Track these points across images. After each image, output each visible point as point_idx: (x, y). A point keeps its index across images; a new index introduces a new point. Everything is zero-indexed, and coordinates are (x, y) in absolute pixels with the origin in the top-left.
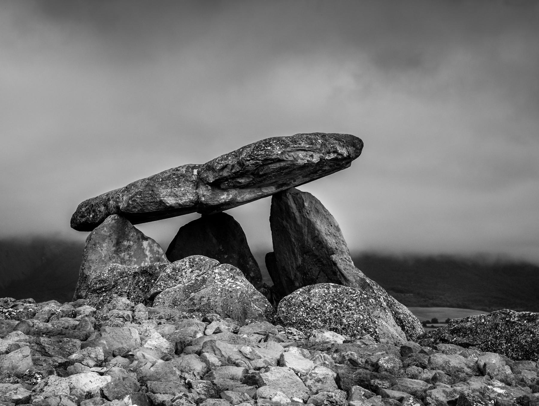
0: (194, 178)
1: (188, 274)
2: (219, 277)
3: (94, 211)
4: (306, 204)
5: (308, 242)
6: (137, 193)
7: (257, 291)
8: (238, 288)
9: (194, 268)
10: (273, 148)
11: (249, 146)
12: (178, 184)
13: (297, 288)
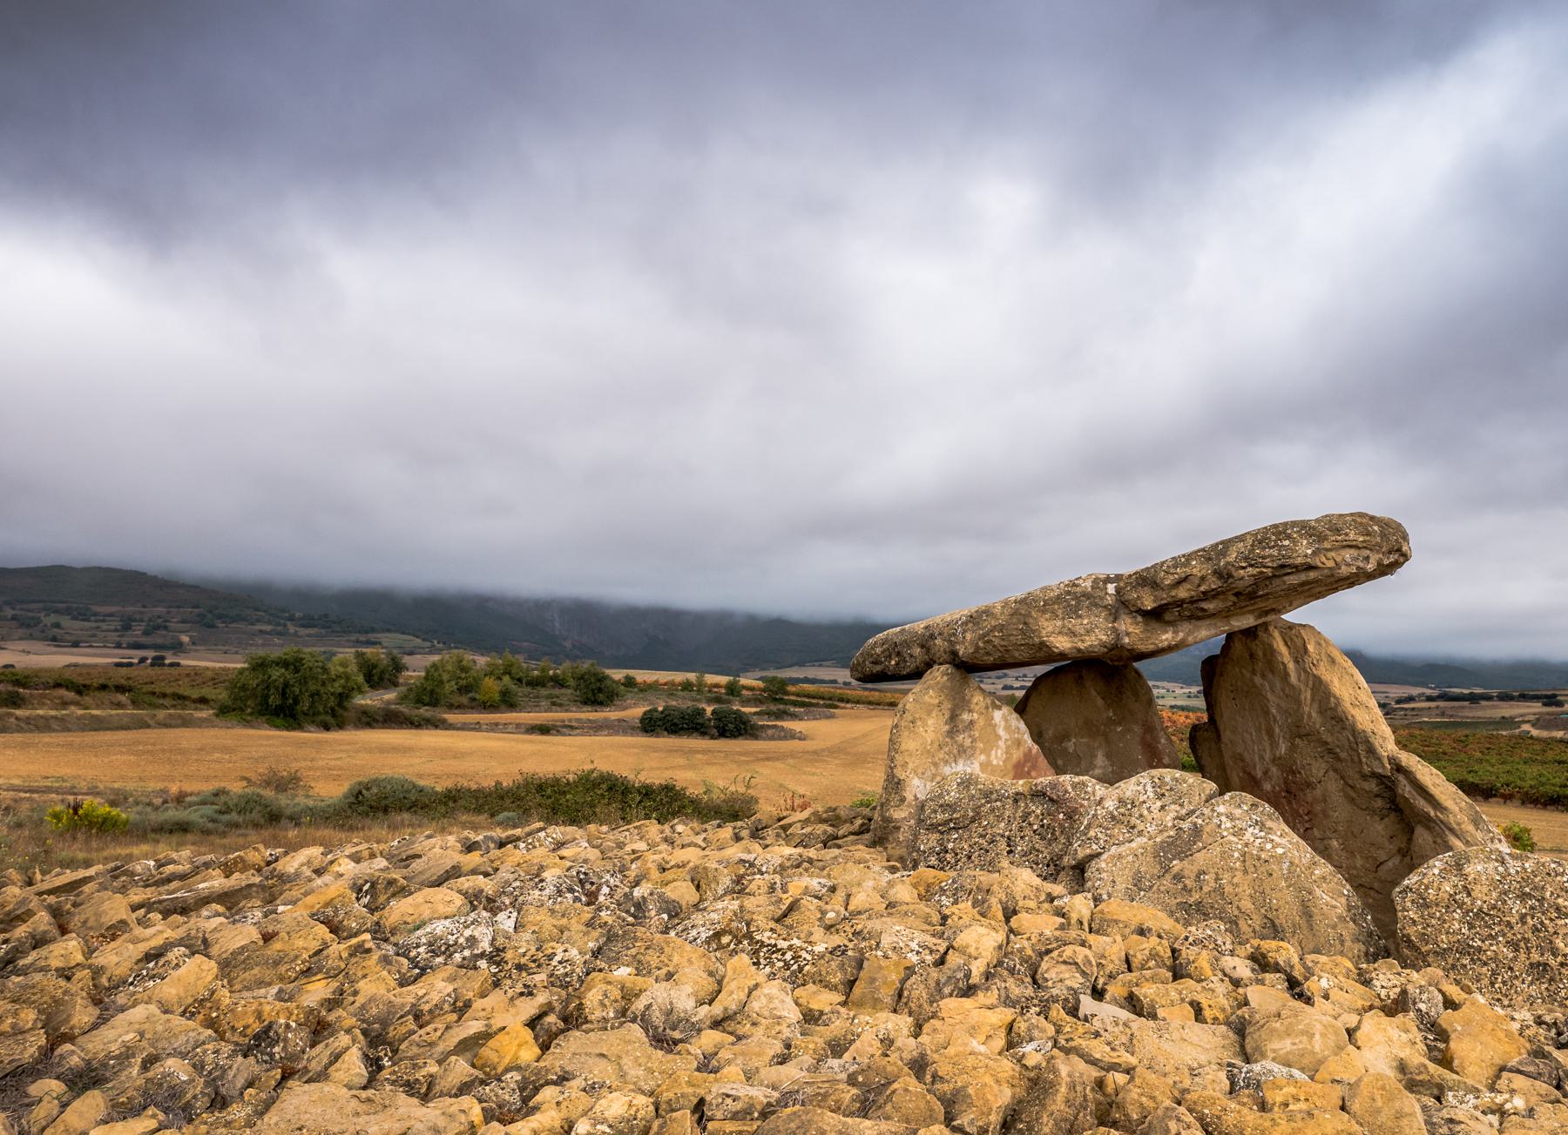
0: (1109, 600)
1: (1156, 814)
2: (1229, 825)
3: (898, 654)
4: (1311, 648)
5: (1310, 716)
6: (993, 629)
7: (1317, 858)
8: (1280, 851)
9: (1166, 800)
10: (1294, 542)
11: (1241, 538)
12: (1076, 612)
13: (1425, 858)
